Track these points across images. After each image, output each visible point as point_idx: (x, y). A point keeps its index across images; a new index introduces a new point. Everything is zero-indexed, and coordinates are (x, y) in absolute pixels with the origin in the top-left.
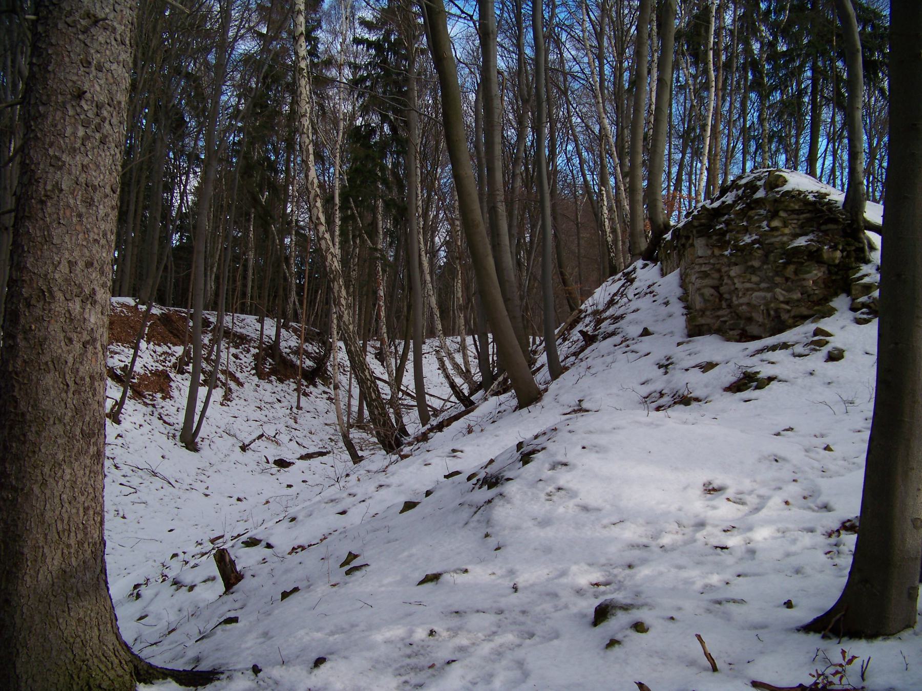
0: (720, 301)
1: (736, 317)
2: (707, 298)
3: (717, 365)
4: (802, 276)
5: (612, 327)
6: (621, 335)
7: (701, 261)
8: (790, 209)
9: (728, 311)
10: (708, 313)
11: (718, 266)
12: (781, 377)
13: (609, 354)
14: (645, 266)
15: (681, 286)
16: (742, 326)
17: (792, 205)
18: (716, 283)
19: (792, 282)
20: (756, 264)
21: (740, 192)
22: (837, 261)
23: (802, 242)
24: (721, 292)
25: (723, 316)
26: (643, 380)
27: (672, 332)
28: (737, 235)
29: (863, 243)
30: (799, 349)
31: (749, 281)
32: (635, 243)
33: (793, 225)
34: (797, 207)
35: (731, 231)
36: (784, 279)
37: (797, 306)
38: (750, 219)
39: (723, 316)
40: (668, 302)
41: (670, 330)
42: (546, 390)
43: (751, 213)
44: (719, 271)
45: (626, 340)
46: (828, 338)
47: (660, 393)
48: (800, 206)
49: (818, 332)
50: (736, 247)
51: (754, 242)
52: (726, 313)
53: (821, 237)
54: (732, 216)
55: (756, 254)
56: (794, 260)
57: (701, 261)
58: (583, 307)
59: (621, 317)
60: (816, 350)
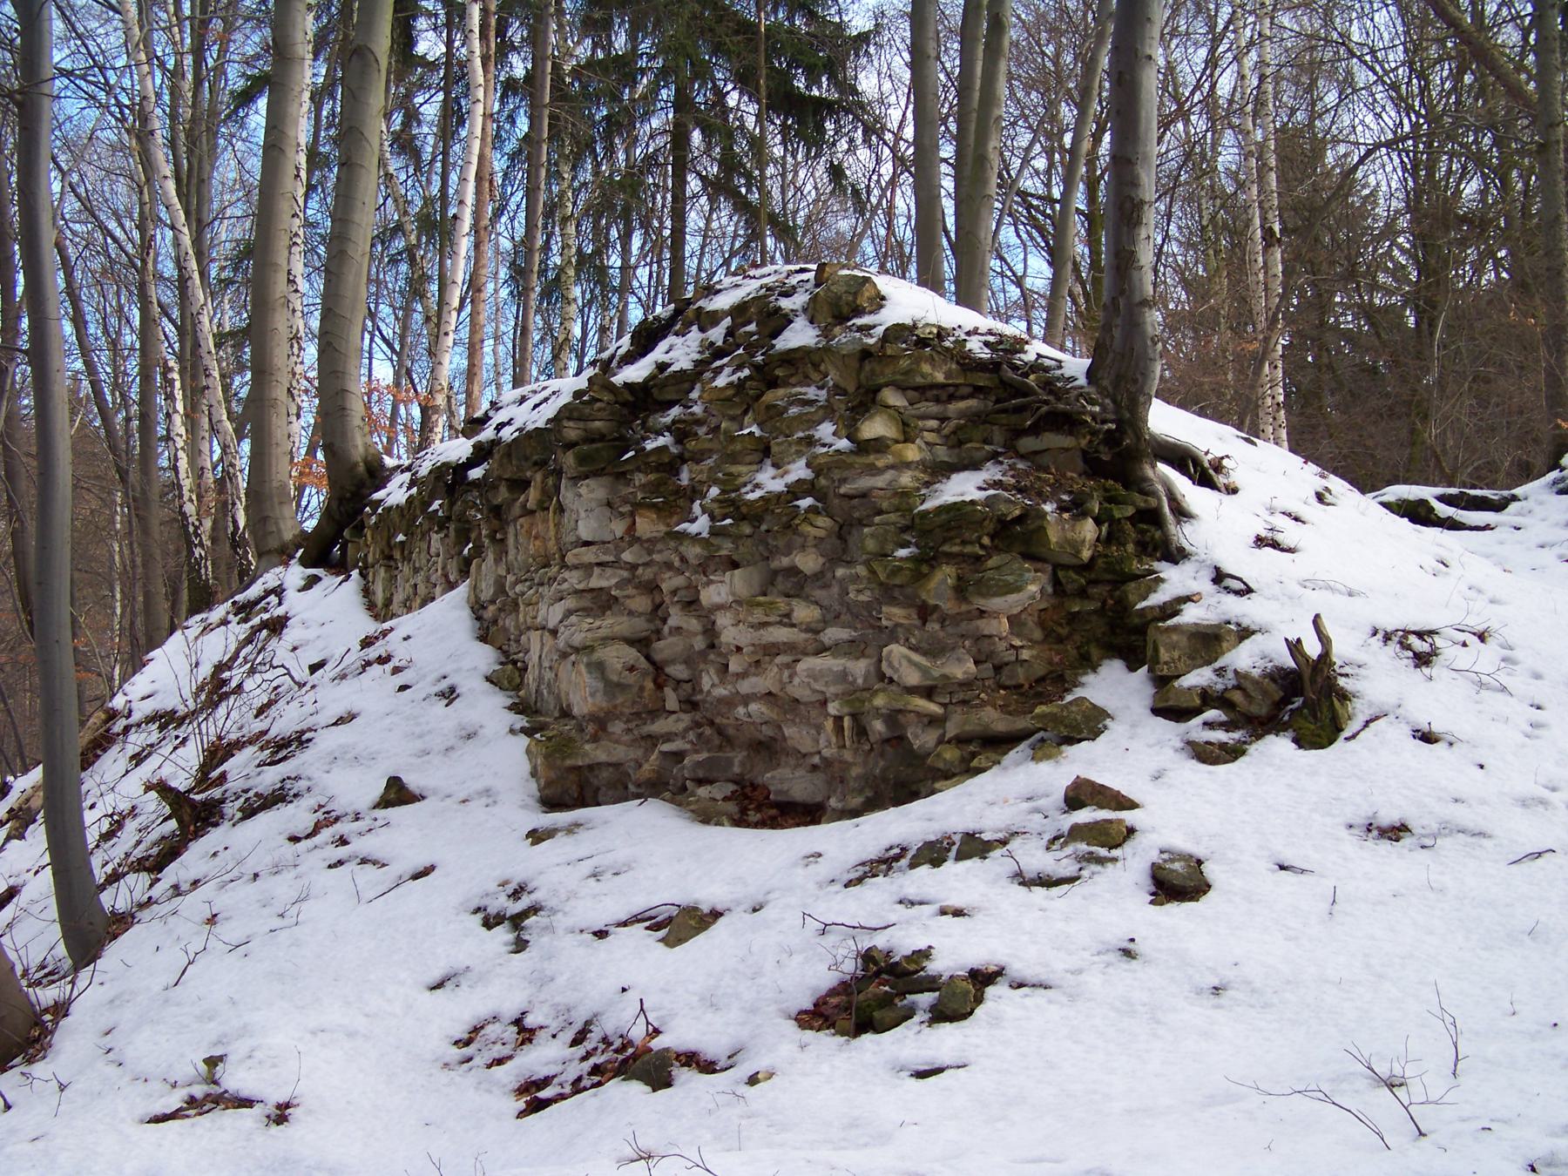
0: (659, 687)
1: (717, 741)
2: (615, 678)
3: (716, 915)
4: (981, 603)
5: (270, 778)
6: (308, 802)
7: (589, 555)
8: (919, 380)
9: (686, 719)
10: (617, 727)
11: (645, 574)
12: (1017, 968)
13: (277, 870)
14: (312, 582)
15: (483, 638)
16: (737, 769)
17: (926, 368)
18: (640, 626)
19: (942, 621)
20: (808, 562)
21: (717, 334)
22: (1086, 554)
23: (964, 488)
24: (657, 657)
25: (668, 737)
26: (435, 975)
27: (487, 792)
28: (735, 469)
29: (1154, 494)
30: (1035, 858)
31: (786, 620)
32: (264, 520)
33: (929, 437)
34: (940, 377)
35: (697, 458)
36: (914, 613)
37: (964, 702)
38: (772, 416)
39: (668, 737)
40: (452, 689)
41: (480, 785)
42: (61, 1009)
43: (775, 396)
44: (652, 588)
45: (330, 820)
46: (1128, 816)
47: (518, 1022)
48: (948, 375)
49: (1080, 794)
50: (731, 505)
51: (796, 490)
52: (681, 726)
53: (1027, 474)
54: (697, 409)
55: (806, 528)
56: (946, 548)
57: (589, 555)
58: (118, 702)
59: (300, 740)
60: (1101, 861)
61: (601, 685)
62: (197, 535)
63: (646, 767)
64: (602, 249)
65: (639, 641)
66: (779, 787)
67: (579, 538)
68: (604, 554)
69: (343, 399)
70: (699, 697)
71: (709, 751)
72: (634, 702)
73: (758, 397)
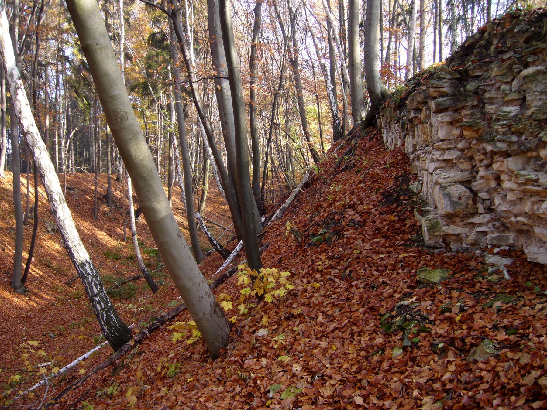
0: (475, 202)
9: (488, 217)
16: (511, 241)
18: (466, 175)
25: (480, 225)
39: (480, 225)
52: (485, 220)
61: (449, 203)
62: (337, 116)
63: (469, 238)
64: (465, 12)
65: (466, 181)
66: (532, 257)
67: (439, 138)
68: (450, 144)
69: (373, 73)
70: (493, 207)
71: (498, 232)
72: (464, 210)
73: (519, 73)
